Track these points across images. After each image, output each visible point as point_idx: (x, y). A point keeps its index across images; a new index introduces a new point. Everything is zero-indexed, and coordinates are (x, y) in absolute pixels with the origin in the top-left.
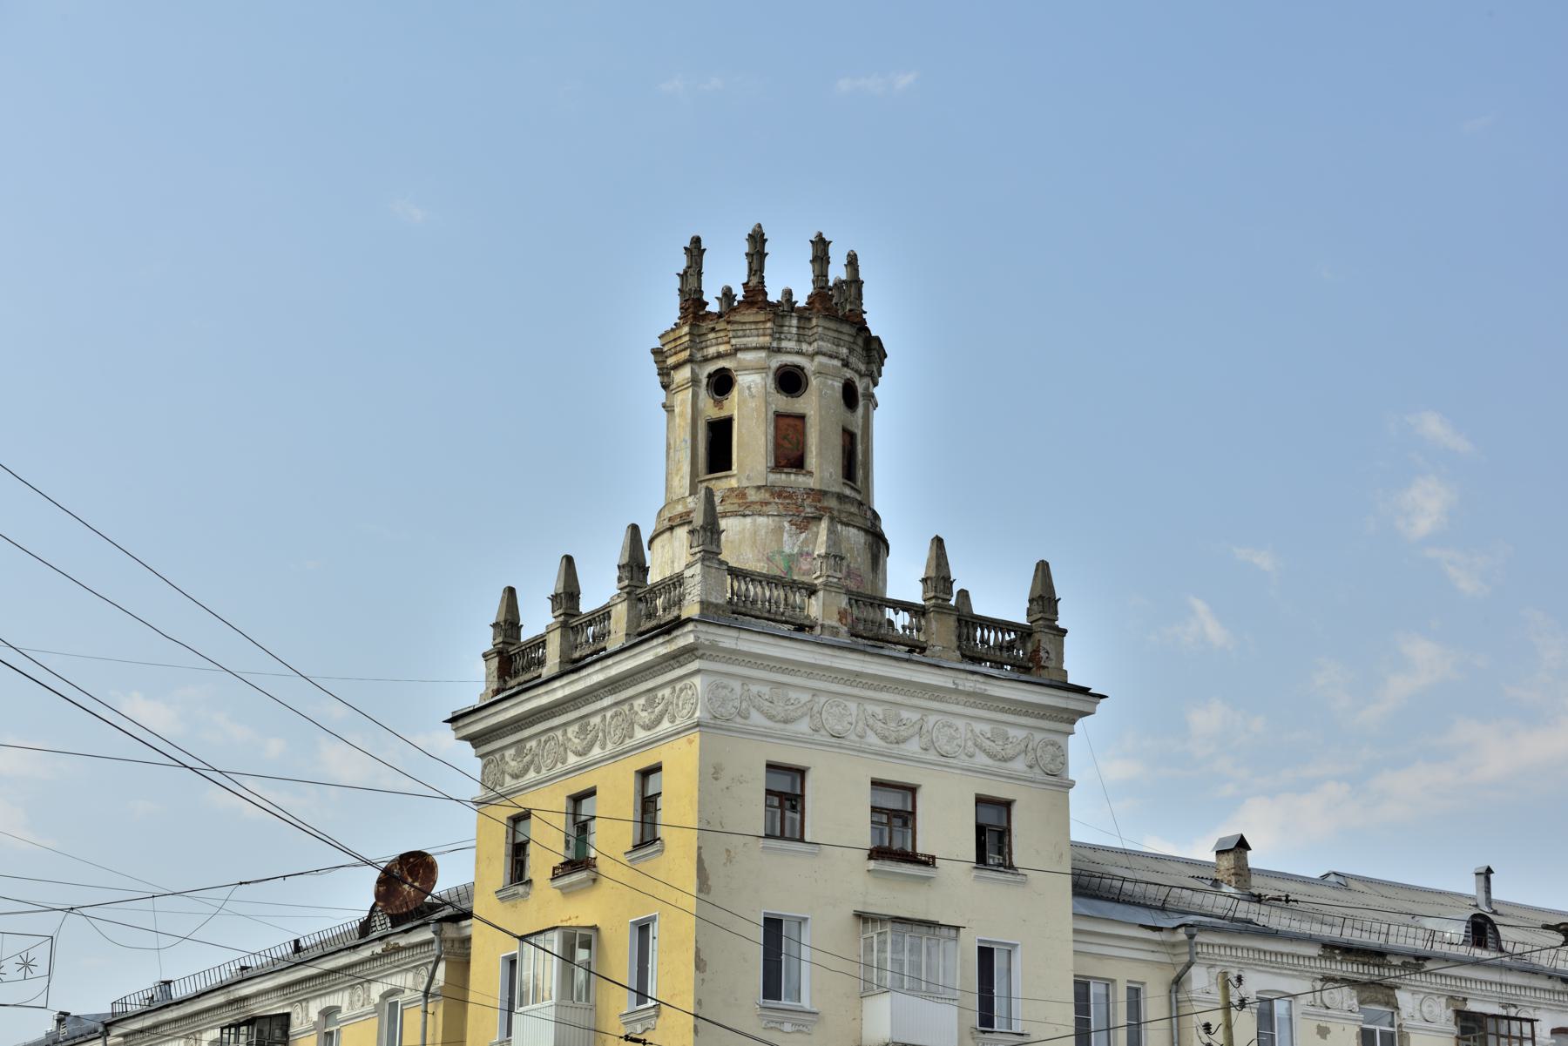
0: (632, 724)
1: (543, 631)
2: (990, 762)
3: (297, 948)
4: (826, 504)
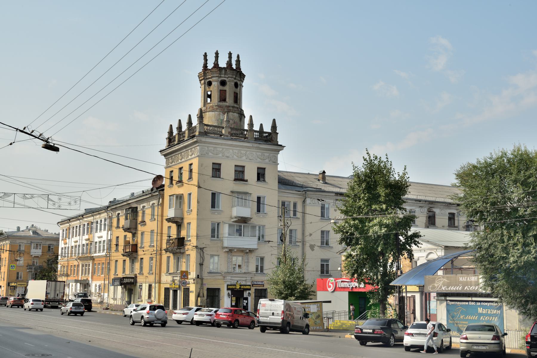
3: (143, 192)
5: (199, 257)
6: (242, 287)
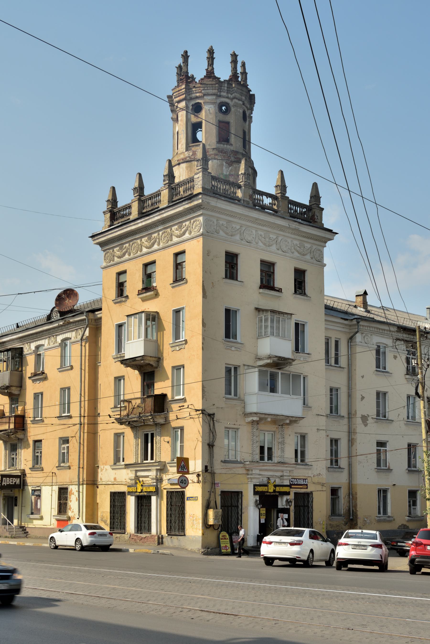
0: (172, 235)
1: (130, 201)
2: (299, 255)
4: (238, 156)
5: (207, 430)
6: (278, 489)
